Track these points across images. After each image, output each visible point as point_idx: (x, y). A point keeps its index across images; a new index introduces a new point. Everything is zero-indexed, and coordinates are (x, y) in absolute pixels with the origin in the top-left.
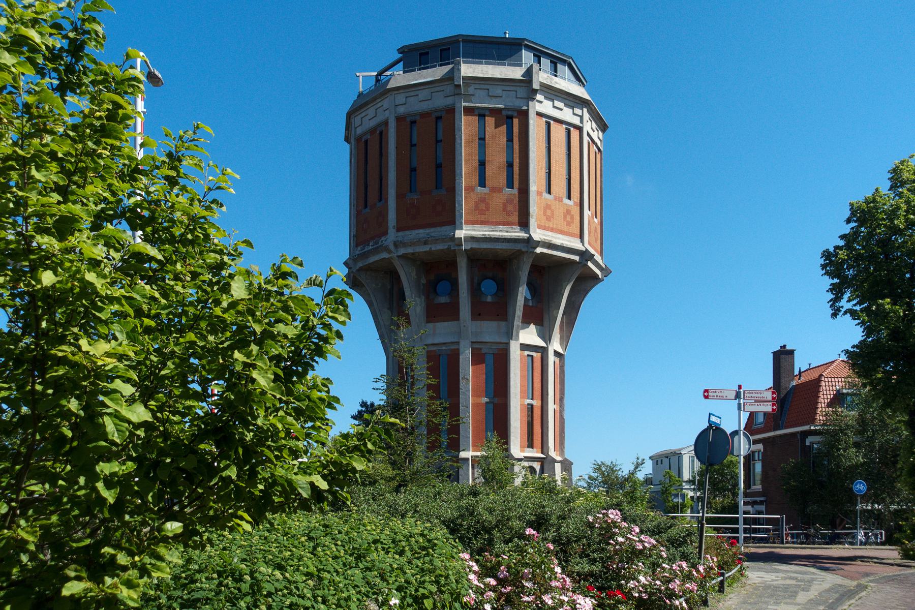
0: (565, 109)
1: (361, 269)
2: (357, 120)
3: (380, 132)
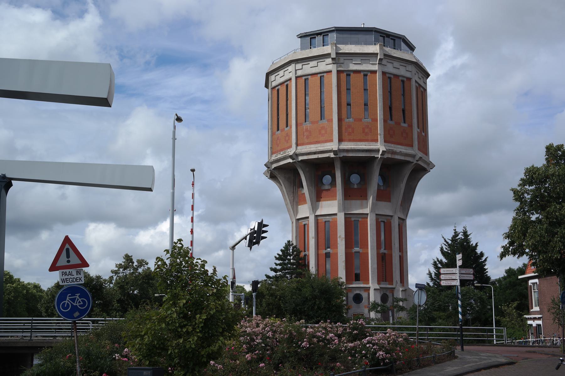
0: (401, 68)
1: (275, 168)
2: (272, 78)
3: (286, 84)
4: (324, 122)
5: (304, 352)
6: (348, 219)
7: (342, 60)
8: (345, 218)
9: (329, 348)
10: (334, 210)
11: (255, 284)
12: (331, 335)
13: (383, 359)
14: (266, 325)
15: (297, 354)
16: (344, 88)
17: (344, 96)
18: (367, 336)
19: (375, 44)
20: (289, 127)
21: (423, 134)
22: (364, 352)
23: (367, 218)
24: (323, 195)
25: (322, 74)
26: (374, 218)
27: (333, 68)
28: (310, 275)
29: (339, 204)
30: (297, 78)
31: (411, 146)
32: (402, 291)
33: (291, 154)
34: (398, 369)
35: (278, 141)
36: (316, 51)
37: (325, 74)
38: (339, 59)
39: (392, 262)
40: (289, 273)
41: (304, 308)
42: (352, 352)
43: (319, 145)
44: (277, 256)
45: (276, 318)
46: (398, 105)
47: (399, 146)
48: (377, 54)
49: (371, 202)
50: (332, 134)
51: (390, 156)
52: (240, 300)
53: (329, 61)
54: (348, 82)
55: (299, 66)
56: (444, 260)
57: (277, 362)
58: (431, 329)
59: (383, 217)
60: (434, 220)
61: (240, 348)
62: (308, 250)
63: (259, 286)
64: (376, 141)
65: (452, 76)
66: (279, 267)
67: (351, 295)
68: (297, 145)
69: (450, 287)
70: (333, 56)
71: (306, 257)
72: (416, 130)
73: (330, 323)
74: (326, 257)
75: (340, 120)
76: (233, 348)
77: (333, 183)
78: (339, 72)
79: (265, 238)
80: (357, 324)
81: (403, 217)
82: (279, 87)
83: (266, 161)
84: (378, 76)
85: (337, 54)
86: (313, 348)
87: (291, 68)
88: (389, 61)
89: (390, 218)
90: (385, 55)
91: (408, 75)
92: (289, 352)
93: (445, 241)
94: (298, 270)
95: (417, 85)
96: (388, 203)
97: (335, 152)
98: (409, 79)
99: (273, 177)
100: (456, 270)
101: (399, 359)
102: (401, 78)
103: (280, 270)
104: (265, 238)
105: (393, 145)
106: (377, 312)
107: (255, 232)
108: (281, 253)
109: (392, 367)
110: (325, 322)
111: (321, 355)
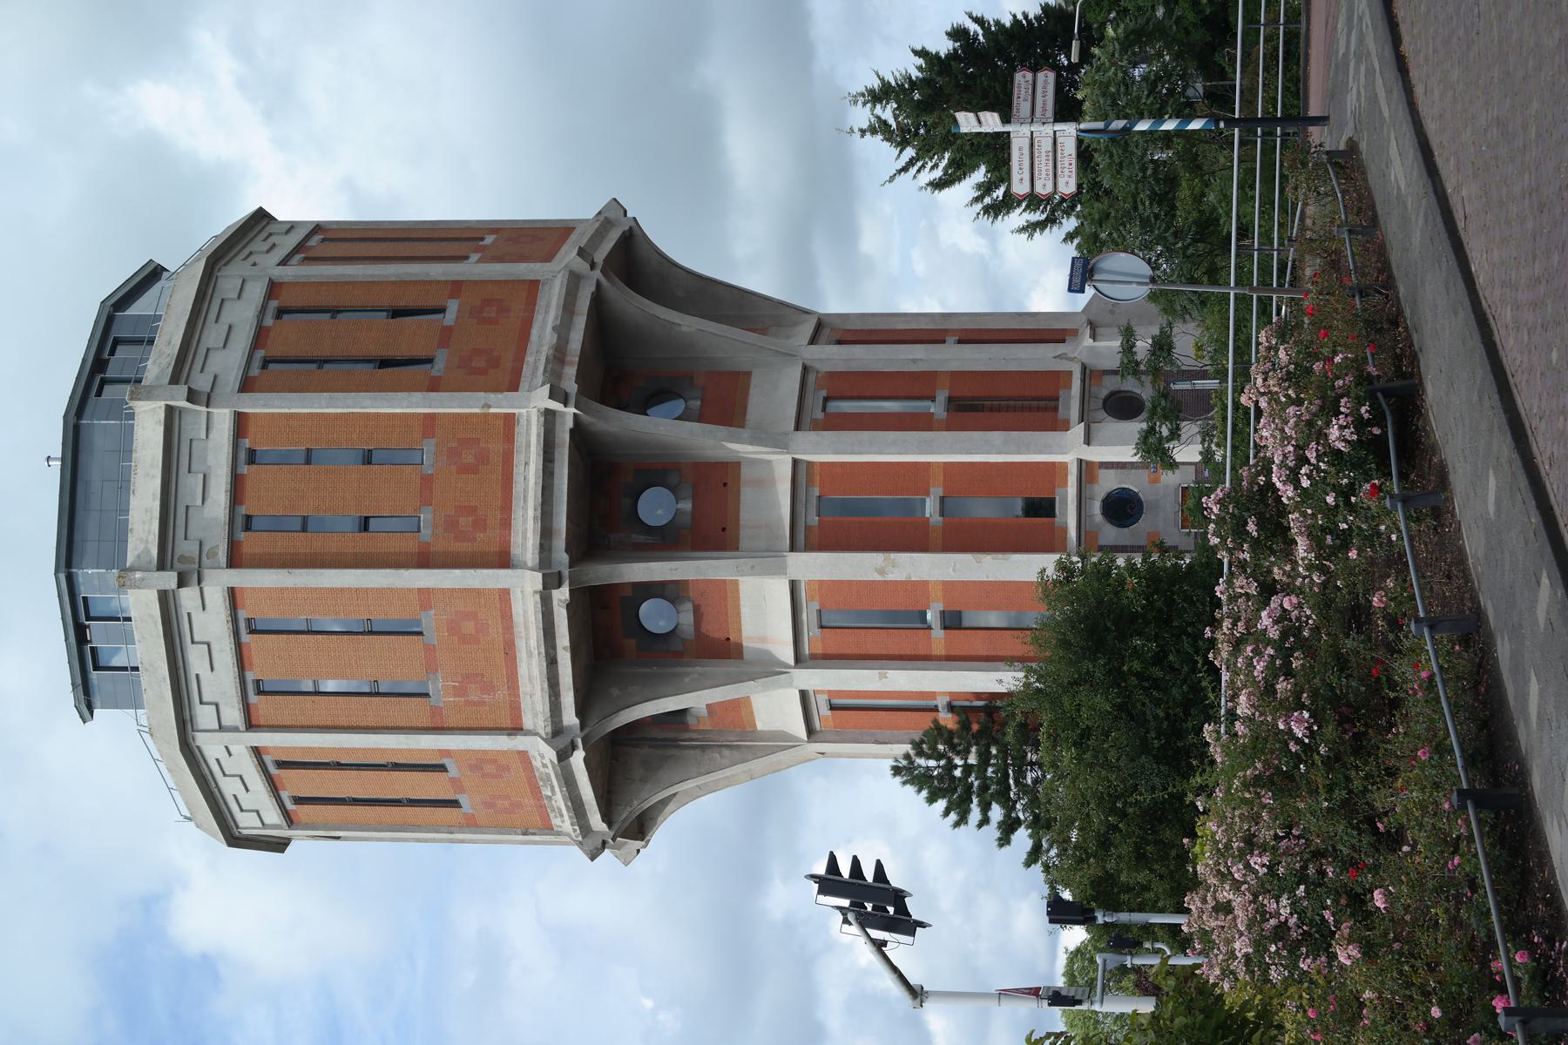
0: (226, 318)
1: (607, 817)
2: (247, 823)
3: (273, 769)
4: (429, 621)
5: (1330, 730)
6: (806, 539)
7: (187, 548)
8: (809, 547)
9: (1316, 630)
10: (776, 593)
11: (1060, 913)
12: (1265, 620)
13: (1360, 424)
14: (1224, 876)
15: (1337, 759)
16: (300, 543)
17: (333, 544)
18: (1270, 485)
19: (132, 416)
20: (445, 761)
21: (489, 239)
22: (1330, 500)
23: (810, 464)
24: (718, 635)
25: (242, 625)
26: (812, 436)
27: (218, 582)
28: (1028, 693)
29: (754, 571)
30: (251, 725)
31: (533, 286)
32: (1094, 337)
33: (551, 754)
34: (1398, 368)
35: (499, 803)
36: (146, 647)
37: (243, 615)
38: (183, 559)
39: (988, 377)
40: (1020, 775)
41: (1156, 717)
42: (1331, 542)
43: (520, 644)
44: (953, 817)
45: (1193, 835)
46: (376, 335)
47: (535, 332)
48: (170, 410)
49: (750, 448)
50: (478, 593)
51: (571, 371)
52: (1123, 970)
53: (188, 598)
54: (277, 526)
55: (204, 716)
56: (980, 175)
57: (1366, 839)
58: (1244, 232)
60: (823, 202)
61: (1311, 982)
62: (932, 695)
63: (1067, 895)
64: (510, 421)
65: (276, 96)
66: (996, 813)
67: (1110, 534)
68: (517, 729)
69: (1084, 155)
70: (169, 580)
71: (962, 708)
72: (474, 269)
73: (1215, 624)
74: (959, 628)
75: (424, 560)
76: (1310, 1013)
77: (669, 591)
78: (234, 561)
79: (879, 867)
80: (1220, 521)
81: (808, 329)
82: (285, 795)
83: (577, 854)
84: (259, 405)
85: (161, 566)
86: (1314, 695)
87: (211, 747)
88: (198, 366)
89: (811, 378)
90: (175, 380)
91: (256, 291)
92: (1330, 789)
93: (905, 169)
94: (1010, 738)
95: (298, 257)
96: (754, 381)
97: (551, 581)
98: (274, 288)
99: (639, 829)
100: (1019, 134)
101: (1357, 365)
102: (269, 321)
103: (1009, 806)
104: (879, 867)
105: (529, 359)
106: (1175, 434)
107: (857, 906)
108: (941, 804)
109: (1387, 393)
110: (1212, 643)
111: (1342, 663)
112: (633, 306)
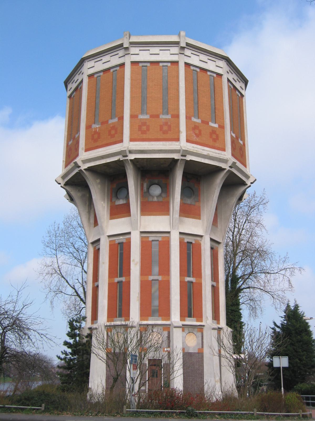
4: (116, 120)
59: (190, 237)
64: (178, 139)
96: (198, 220)
98: (220, 75)
112: (219, 180)
